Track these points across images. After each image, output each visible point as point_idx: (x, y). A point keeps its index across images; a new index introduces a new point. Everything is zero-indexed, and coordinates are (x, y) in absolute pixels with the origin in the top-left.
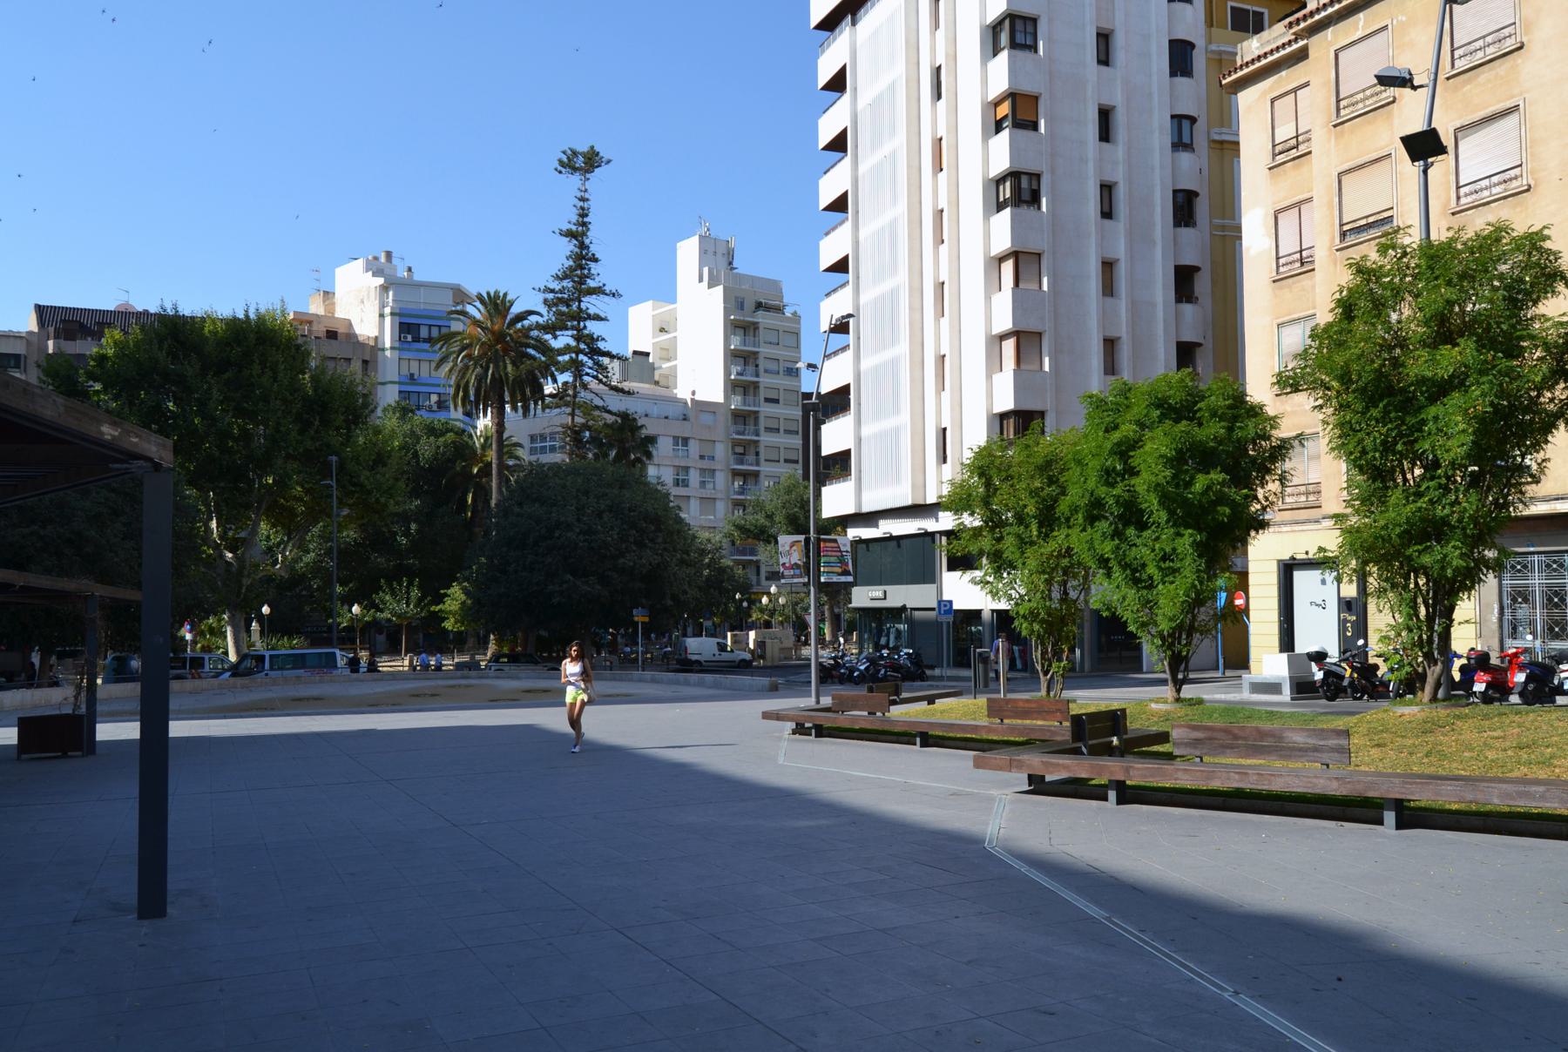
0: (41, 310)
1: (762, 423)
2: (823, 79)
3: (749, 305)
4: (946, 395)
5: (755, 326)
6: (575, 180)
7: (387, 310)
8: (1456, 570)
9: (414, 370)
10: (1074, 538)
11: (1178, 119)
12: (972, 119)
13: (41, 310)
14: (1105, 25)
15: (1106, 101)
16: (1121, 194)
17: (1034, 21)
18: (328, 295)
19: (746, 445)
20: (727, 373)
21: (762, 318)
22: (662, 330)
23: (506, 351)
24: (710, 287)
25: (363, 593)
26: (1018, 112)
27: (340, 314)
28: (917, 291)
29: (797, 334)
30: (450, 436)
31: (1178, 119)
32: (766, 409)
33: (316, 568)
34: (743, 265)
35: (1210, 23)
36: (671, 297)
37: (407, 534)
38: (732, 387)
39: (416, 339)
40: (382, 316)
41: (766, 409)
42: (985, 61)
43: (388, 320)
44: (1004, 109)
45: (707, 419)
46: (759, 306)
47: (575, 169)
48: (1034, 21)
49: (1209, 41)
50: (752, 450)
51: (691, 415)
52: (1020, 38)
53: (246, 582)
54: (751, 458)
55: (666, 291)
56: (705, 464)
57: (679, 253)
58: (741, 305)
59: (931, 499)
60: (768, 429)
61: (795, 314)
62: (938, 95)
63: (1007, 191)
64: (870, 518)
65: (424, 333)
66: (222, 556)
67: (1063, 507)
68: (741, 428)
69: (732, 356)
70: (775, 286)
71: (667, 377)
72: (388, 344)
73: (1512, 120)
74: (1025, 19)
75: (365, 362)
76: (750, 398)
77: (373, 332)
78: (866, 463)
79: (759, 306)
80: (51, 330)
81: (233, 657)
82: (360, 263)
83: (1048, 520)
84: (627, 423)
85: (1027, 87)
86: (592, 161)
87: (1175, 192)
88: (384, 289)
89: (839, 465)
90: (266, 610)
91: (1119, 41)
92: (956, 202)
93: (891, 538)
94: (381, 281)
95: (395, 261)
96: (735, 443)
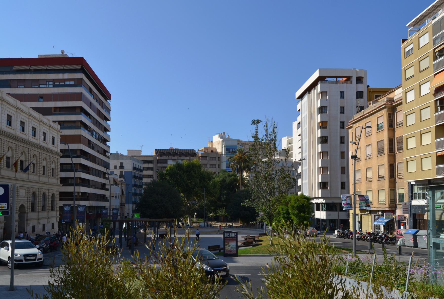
0: (156, 150)
2: (298, 110)
6: (255, 126)
8: (65, 235)
17: (327, 107)
18: (212, 142)
22: (290, 143)
23: (242, 160)
25: (215, 211)
26: (323, 125)
27: (214, 147)
30: (233, 177)
33: (206, 204)
37: (224, 198)
39: (230, 152)
40: (222, 147)
43: (223, 148)
44: (321, 124)
48: (327, 107)
53: (191, 209)
55: (290, 134)
59: (317, 197)
65: (231, 150)
66: (187, 205)
73: (371, 146)
74: (325, 107)
75: (219, 158)
81: (189, 223)
86: (258, 122)
88: (223, 141)
90: (196, 214)
94: (222, 140)
95: (225, 134)
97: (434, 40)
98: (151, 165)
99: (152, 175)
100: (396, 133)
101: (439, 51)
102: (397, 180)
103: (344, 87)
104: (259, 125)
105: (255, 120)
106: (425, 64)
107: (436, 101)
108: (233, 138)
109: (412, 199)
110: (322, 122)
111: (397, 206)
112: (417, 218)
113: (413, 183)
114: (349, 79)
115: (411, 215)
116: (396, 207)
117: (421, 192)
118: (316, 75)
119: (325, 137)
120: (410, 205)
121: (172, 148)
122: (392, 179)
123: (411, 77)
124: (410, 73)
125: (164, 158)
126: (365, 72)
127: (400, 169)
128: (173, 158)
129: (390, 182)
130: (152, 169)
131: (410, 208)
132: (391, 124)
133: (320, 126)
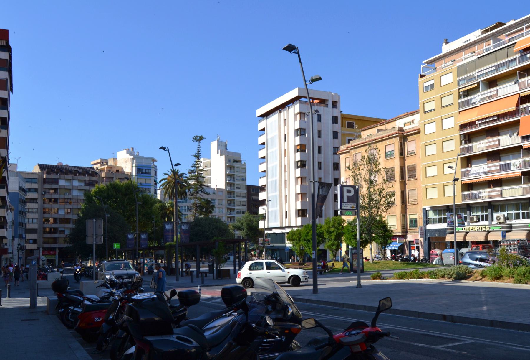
0: (40, 165)
1: (236, 195)
3: (232, 161)
4: (287, 204)
5: (234, 167)
6: (197, 143)
7: (134, 165)
9: (141, 182)
10: (302, 243)
11: (335, 148)
12: (292, 165)
13: (40, 165)
14: (319, 129)
15: (320, 145)
16: (323, 164)
17: (305, 129)
19: (231, 201)
20: (226, 180)
21: (236, 165)
24: (221, 155)
27: (118, 165)
28: (281, 181)
29: (245, 169)
31: (335, 148)
32: (237, 191)
34: (230, 149)
35: (342, 126)
36: (209, 158)
38: (227, 184)
40: (132, 166)
41: (237, 191)
42: (295, 137)
43: (134, 168)
45: (220, 193)
46: (235, 161)
47: (197, 140)
48: (305, 129)
49: (342, 130)
50: (233, 202)
51: (216, 193)
52: (302, 133)
54: (232, 204)
56: (220, 206)
57: (211, 145)
58: (229, 161)
59: (284, 226)
60: (238, 196)
61: (244, 163)
62: (285, 140)
63: (299, 164)
64: (271, 229)
65: (144, 171)
67: (301, 239)
68: (229, 196)
69: (227, 176)
70: (239, 155)
71: (207, 180)
72: (134, 174)
74: (303, 129)
76: (232, 187)
77: (130, 171)
78: (270, 217)
79: (235, 161)
80: (45, 172)
82: (125, 151)
83: (300, 241)
84: (208, 202)
85: (303, 143)
86: (201, 138)
87: (334, 163)
88: (133, 159)
89: (264, 217)
91: (322, 133)
92: (288, 133)
93: (275, 233)
94: (132, 157)
95: (134, 150)
96: (228, 200)
97: (459, 81)
98: (35, 186)
99: (36, 199)
100: (406, 162)
101: (463, 91)
102: (408, 206)
103: (321, 109)
104: (201, 141)
105: (197, 137)
106: (446, 101)
107: (461, 135)
108: (145, 156)
109: (427, 224)
110: (300, 145)
111: (408, 231)
112: (431, 241)
113: (428, 209)
114: (323, 102)
115: (426, 239)
116: (407, 232)
117: (437, 217)
118: (294, 93)
119: (304, 161)
120: (425, 229)
121: (61, 163)
122: (404, 205)
123: (430, 111)
124: (428, 107)
125: (53, 176)
126: (339, 97)
127: (410, 197)
128: (81, 177)
129: (402, 208)
130: (36, 190)
131: (425, 232)
132: (402, 153)
133: (298, 150)
